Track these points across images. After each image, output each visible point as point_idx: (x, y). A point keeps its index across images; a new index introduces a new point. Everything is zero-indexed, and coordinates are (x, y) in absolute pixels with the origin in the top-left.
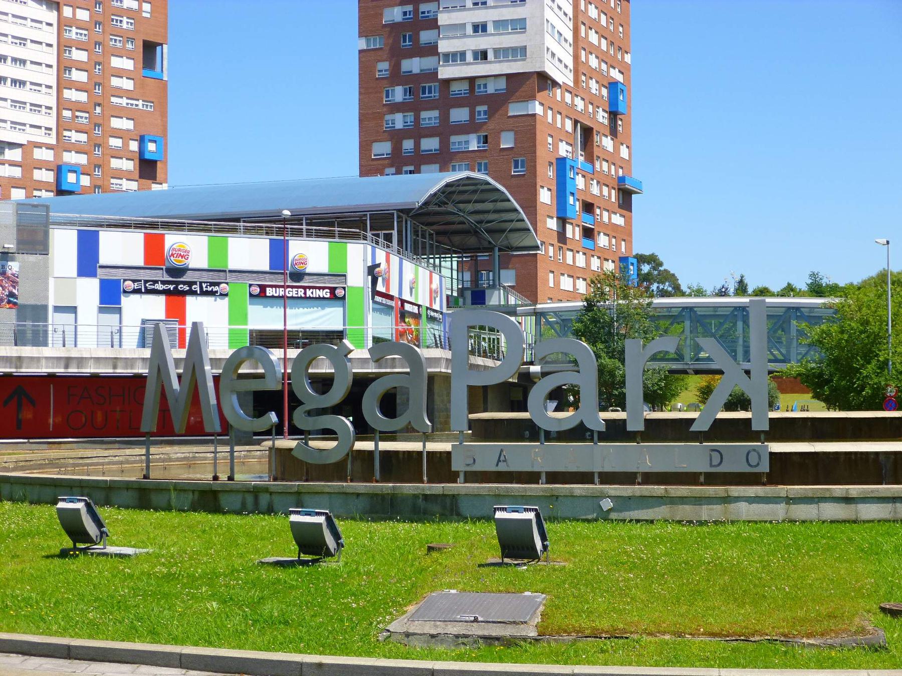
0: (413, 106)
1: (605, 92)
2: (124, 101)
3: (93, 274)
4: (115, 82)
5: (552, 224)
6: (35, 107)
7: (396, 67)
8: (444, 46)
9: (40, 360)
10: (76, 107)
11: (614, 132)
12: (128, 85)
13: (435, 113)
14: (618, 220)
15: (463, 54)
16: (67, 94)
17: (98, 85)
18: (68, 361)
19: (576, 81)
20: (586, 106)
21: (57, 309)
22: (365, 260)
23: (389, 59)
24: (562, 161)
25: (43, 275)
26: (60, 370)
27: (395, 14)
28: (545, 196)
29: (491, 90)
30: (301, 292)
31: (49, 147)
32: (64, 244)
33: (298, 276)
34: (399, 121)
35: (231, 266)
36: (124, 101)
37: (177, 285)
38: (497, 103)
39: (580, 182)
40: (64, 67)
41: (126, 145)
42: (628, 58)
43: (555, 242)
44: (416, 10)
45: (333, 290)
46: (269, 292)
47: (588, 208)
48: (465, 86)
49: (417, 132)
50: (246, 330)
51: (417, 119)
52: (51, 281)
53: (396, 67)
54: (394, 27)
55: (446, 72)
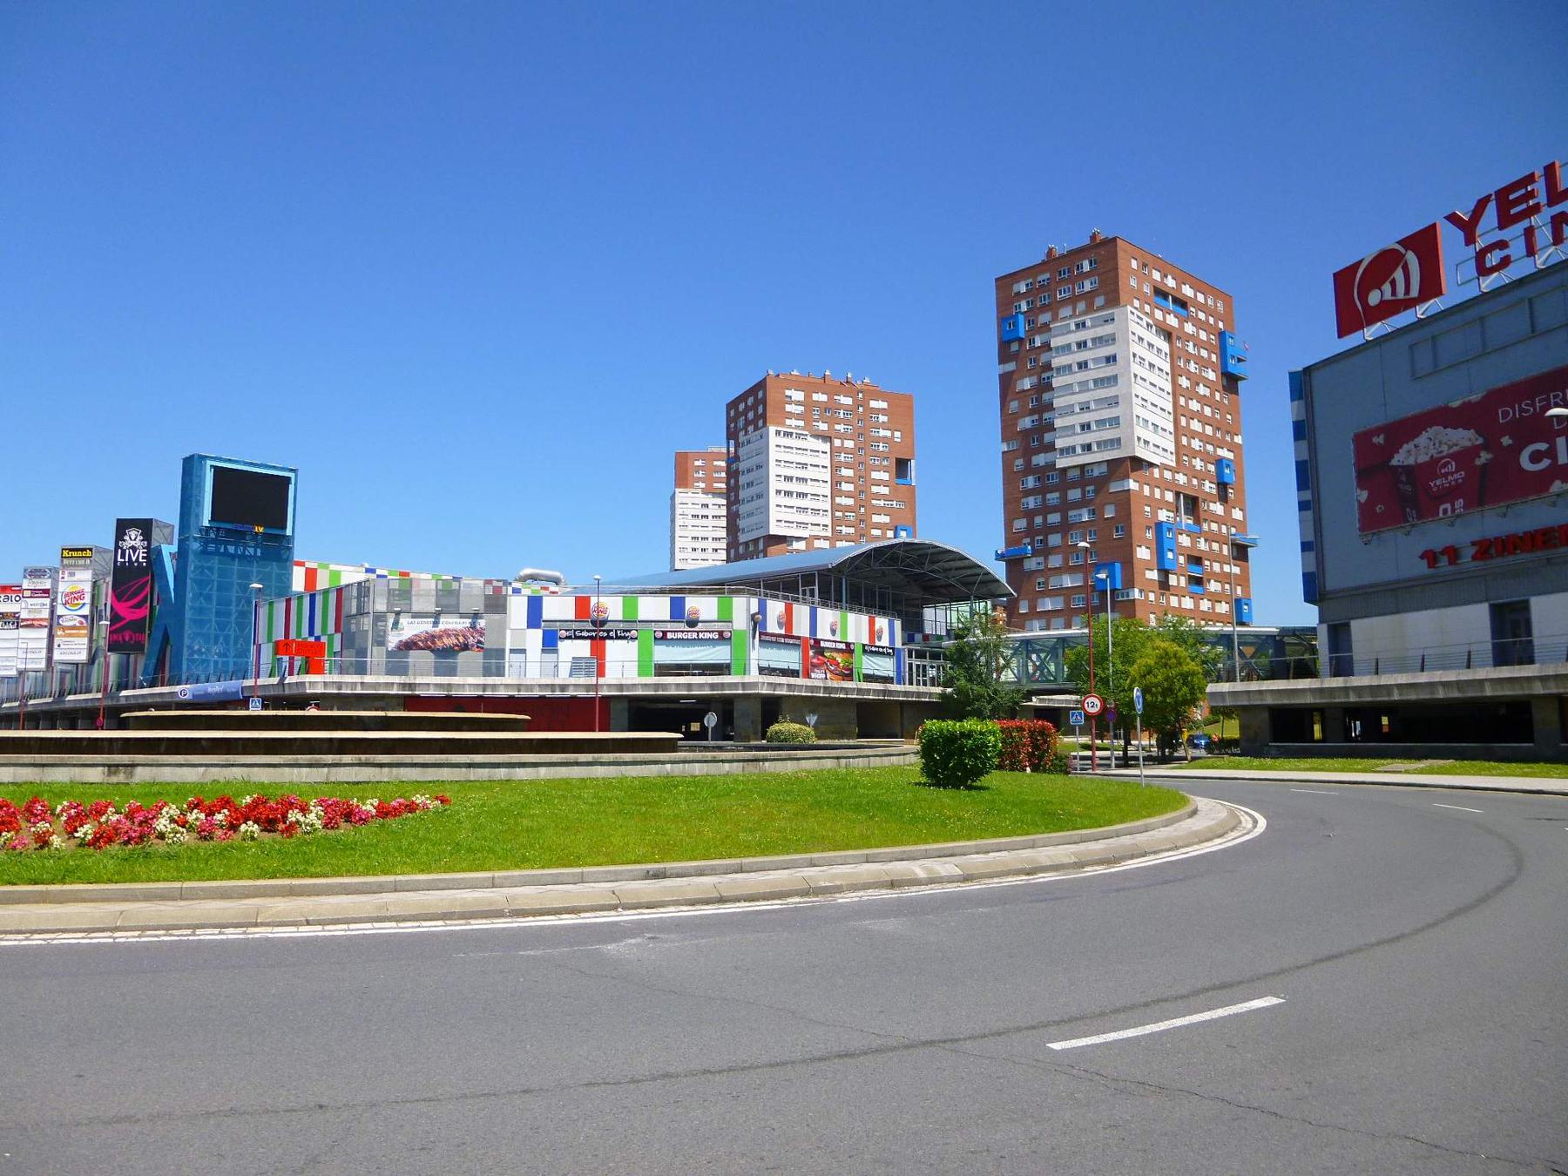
0: (1041, 491)
1: (1212, 468)
2: (882, 503)
3: (538, 626)
4: (875, 489)
5: (1153, 575)
6: (816, 511)
7: (1028, 462)
8: (1059, 444)
9: (505, 684)
10: (847, 509)
11: (1223, 498)
12: (885, 490)
13: (1057, 495)
14: (1236, 570)
15: (1074, 448)
16: (838, 500)
17: (862, 493)
18: (519, 687)
19: (1178, 461)
20: (1189, 481)
21: (512, 651)
22: (748, 609)
23: (1023, 456)
24: (1159, 525)
25: (502, 627)
26: (548, 693)
27: (1026, 423)
28: (1143, 553)
29: (1096, 473)
30: (695, 635)
31: (826, 538)
32: (517, 608)
33: (692, 623)
34: (1031, 502)
35: (641, 617)
36: (882, 503)
37: (598, 632)
38: (1101, 483)
39: (1185, 541)
40: (836, 482)
41: (884, 534)
42: (1238, 439)
43: (1156, 588)
44: (1041, 418)
45: (721, 633)
46: (670, 636)
47: (1196, 560)
48: (1077, 472)
49: (1045, 510)
50: (1543, 663)
51: (1044, 499)
52: (508, 632)
53: (1028, 462)
54: (1026, 432)
55: (1062, 463)
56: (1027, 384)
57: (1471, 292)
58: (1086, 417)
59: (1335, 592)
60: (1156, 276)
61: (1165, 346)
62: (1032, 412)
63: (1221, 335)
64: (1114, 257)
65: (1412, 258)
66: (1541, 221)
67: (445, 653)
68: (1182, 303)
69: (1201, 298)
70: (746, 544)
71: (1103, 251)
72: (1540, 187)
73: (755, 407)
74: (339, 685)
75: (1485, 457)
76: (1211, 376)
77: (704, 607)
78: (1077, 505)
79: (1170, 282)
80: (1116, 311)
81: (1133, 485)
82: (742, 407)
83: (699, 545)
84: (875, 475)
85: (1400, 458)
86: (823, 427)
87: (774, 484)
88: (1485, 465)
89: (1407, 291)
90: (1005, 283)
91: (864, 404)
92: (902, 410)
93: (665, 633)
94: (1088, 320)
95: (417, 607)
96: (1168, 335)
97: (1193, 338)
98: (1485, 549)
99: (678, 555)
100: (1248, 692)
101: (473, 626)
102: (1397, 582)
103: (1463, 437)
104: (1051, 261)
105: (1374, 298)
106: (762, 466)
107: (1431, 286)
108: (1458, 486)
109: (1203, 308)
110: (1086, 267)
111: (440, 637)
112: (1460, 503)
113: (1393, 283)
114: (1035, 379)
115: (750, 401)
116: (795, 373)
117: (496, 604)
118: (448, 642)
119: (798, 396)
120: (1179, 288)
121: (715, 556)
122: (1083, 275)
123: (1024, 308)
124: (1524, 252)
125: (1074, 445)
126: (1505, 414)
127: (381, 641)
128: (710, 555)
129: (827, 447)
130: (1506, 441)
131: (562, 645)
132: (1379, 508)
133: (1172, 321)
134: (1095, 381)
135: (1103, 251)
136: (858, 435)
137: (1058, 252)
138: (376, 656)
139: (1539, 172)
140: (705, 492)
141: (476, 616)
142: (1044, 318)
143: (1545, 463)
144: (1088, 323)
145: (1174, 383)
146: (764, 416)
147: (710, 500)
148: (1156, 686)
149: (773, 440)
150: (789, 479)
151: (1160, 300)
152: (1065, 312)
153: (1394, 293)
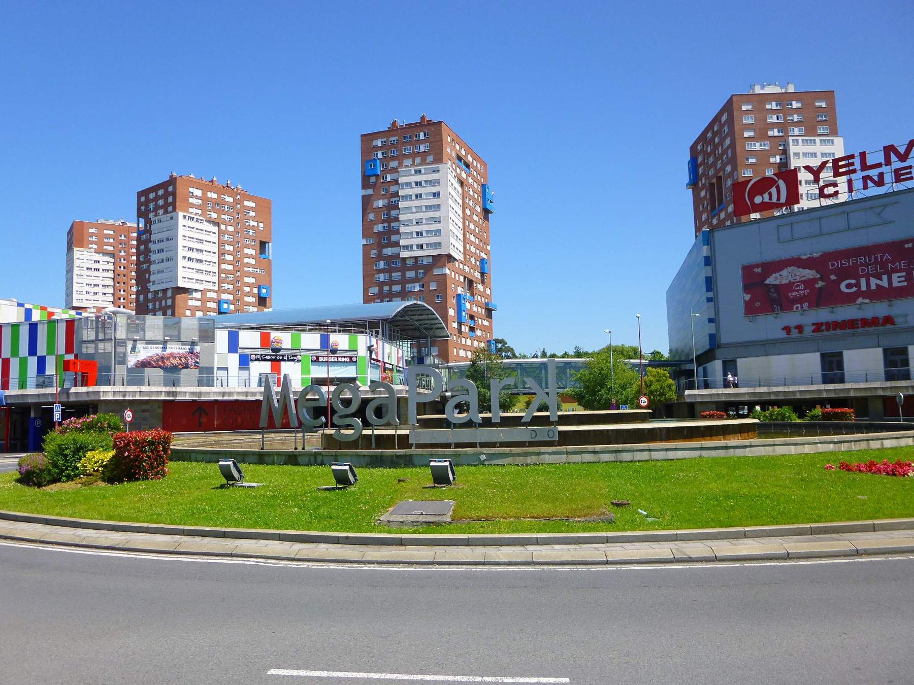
0: (388, 270)
1: (478, 263)
5: (455, 325)
6: (208, 272)
7: (380, 253)
9: (211, 393)
10: (227, 272)
11: (483, 282)
12: (253, 262)
13: (399, 274)
14: (486, 323)
17: (238, 262)
18: (224, 394)
19: (465, 258)
21: (219, 369)
25: (212, 352)
27: (379, 228)
28: (451, 312)
29: (425, 262)
31: (214, 291)
32: (222, 338)
33: (334, 351)
34: (382, 277)
37: (276, 357)
38: (428, 268)
39: (468, 305)
40: (221, 253)
42: (489, 248)
44: (389, 226)
45: (351, 358)
46: (321, 359)
47: (472, 317)
49: (391, 283)
52: (216, 356)
53: (380, 253)
54: (379, 233)
55: (403, 254)
56: (381, 203)
57: (815, 204)
58: (419, 228)
59: (724, 344)
60: (458, 147)
61: (460, 189)
62: (383, 222)
63: (483, 186)
64: (440, 133)
65: (781, 183)
66: (857, 177)
67: (171, 370)
68: (467, 165)
69: (475, 163)
70: (156, 292)
71: (431, 130)
72: (857, 161)
73: (165, 197)
74: (124, 394)
75: (820, 284)
76: (479, 209)
77: (341, 340)
78: (412, 281)
79: (463, 153)
80: (441, 166)
81: (448, 272)
82: (152, 196)
83: (92, 289)
84: (247, 251)
85: (770, 280)
86: (214, 215)
87: (181, 252)
88: (820, 288)
89: (779, 199)
90: (367, 139)
91: (240, 203)
92: (264, 208)
93: (317, 357)
94: (422, 168)
95: (149, 335)
96: (462, 183)
97: (471, 186)
98: (818, 327)
99: (75, 296)
100: (702, 395)
101: (191, 352)
102: (767, 340)
103: (809, 274)
104: (394, 129)
105: (758, 200)
106: (172, 239)
107: (794, 197)
108: (805, 296)
109: (476, 170)
110: (422, 136)
111: (168, 359)
112: (805, 305)
113: (770, 194)
114: (386, 201)
115: (161, 192)
116: (192, 176)
117: (207, 335)
118: (174, 362)
119: (198, 193)
120: (466, 156)
121: (104, 298)
122: (420, 139)
123: (380, 156)
124: (847, 190)
125: (411, 243)
126: (833, 265)
127: (123, 361)
128: (100, 297)
129: (216, 229)
130: (833, 277)
131: (253, 365)
132: (757, 304)
133: (464, 175)
134: (426, 207)
135: (431, 130)
136: (237, 223)
137: (400, 123)
138: (120, 371)
139: (857, 154)
140: (97, 252)
141: (193, 343)
142: (393, 164)
143: (855, 289)
144: (423, 171)
145: (464, 212)
146: (174, 204)
147: (100, 257)
148: (656, 391)
149: (181, 222)
150: (191, 249)
151: (458, 161)
152: (408, 162)
153: (770, 198)
